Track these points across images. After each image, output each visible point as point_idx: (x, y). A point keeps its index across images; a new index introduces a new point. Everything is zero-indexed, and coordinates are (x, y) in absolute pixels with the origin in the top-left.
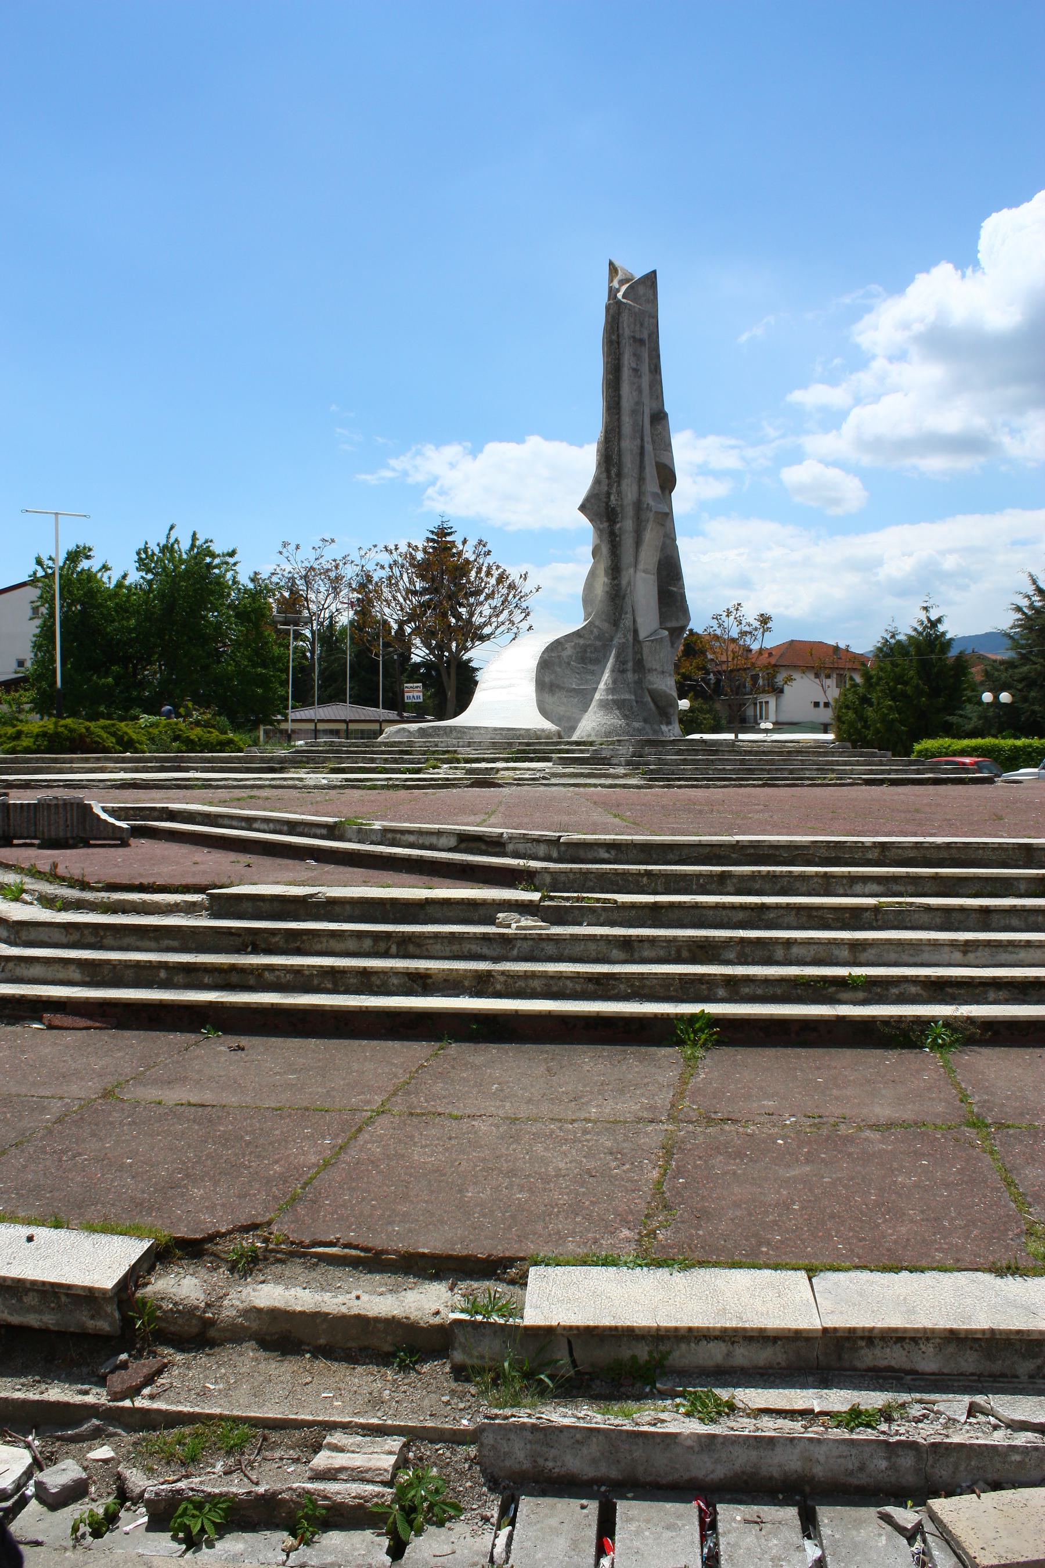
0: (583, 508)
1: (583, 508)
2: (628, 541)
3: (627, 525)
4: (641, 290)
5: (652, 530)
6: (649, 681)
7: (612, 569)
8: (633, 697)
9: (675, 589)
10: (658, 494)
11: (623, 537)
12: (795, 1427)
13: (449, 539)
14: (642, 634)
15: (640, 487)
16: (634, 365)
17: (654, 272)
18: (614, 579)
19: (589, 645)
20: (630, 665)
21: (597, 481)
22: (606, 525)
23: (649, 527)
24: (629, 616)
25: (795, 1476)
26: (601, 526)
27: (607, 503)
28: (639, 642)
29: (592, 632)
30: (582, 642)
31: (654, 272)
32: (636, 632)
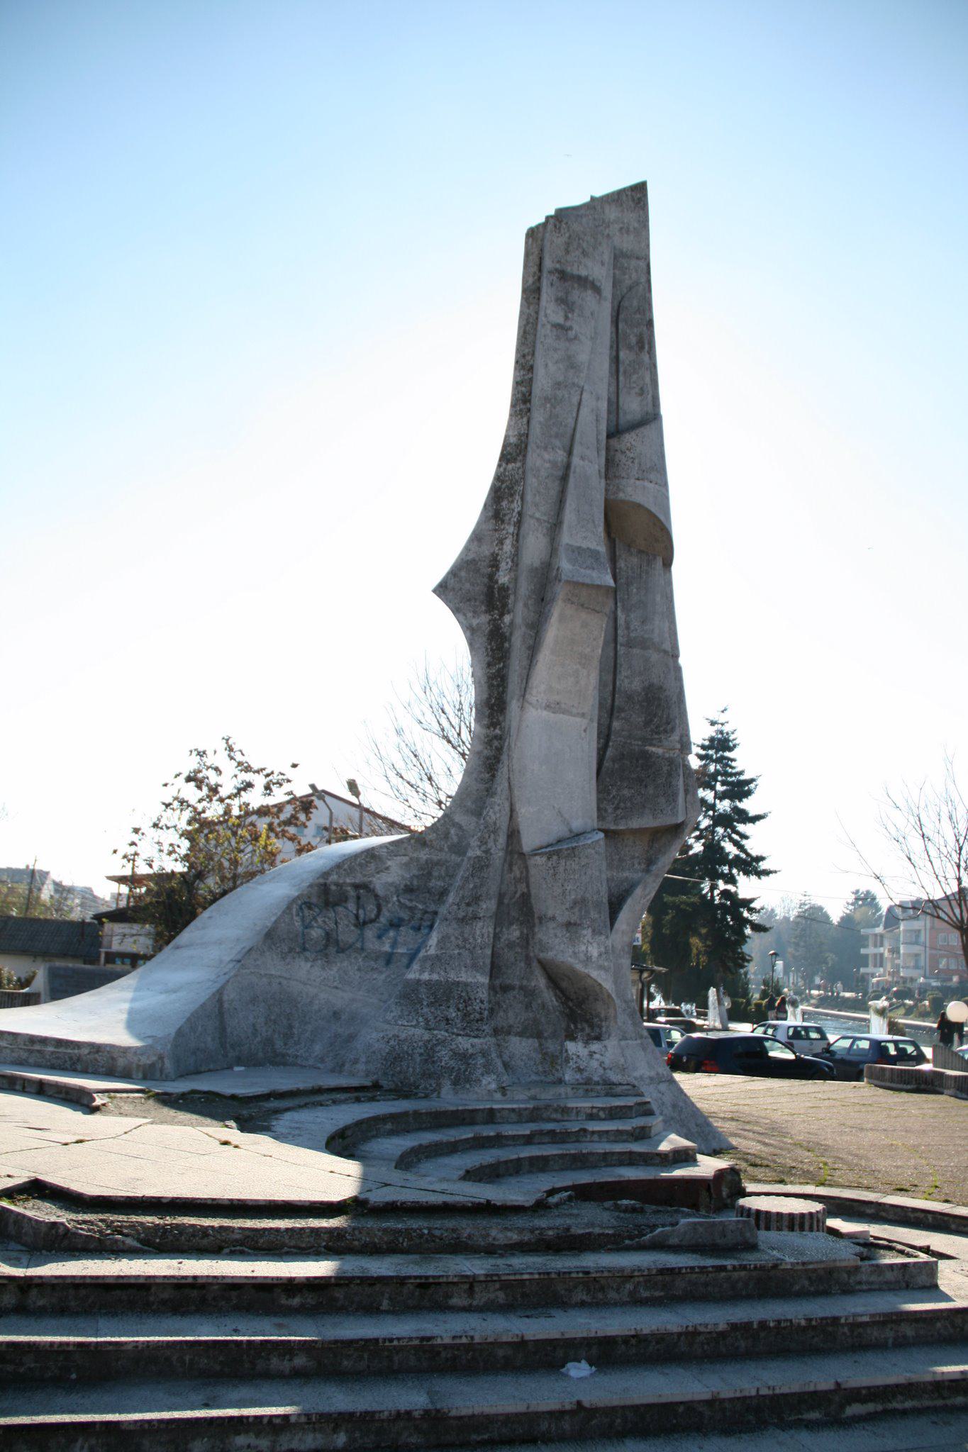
0: (443, 590)
1: (443, 590)
2: (518, 643)
3: (519, 614)
4: (612, 213)
5: (562, 619)
6: (540, 941)
7: (491, 707)
8: (484, 979)
9: (660, 751)
10: (594, 554)
11: (513, 639)
12: (720, 1090)
13: (727, 754)
14: (529, 841)
15: (562, 991)
16: (559, 319)
17: (636, 196)
18: (493, 725)
19: (438, 863)
20: (488, 906)
21: (476, 537)
22: (484, 618)
23: (560, 602)
24: (505, 769)
25: (410, 1384)
26: (475, 622)
27: (491, 577)
28: (522, 855)
29: (447, 836)
30: (423, 855)
31: (636, 196)
32: (513, 835)
